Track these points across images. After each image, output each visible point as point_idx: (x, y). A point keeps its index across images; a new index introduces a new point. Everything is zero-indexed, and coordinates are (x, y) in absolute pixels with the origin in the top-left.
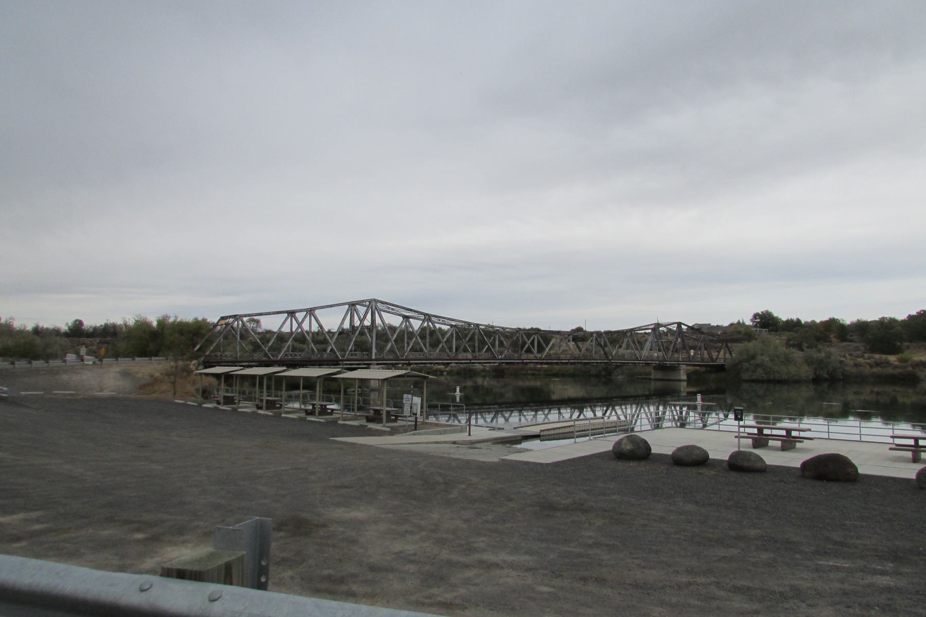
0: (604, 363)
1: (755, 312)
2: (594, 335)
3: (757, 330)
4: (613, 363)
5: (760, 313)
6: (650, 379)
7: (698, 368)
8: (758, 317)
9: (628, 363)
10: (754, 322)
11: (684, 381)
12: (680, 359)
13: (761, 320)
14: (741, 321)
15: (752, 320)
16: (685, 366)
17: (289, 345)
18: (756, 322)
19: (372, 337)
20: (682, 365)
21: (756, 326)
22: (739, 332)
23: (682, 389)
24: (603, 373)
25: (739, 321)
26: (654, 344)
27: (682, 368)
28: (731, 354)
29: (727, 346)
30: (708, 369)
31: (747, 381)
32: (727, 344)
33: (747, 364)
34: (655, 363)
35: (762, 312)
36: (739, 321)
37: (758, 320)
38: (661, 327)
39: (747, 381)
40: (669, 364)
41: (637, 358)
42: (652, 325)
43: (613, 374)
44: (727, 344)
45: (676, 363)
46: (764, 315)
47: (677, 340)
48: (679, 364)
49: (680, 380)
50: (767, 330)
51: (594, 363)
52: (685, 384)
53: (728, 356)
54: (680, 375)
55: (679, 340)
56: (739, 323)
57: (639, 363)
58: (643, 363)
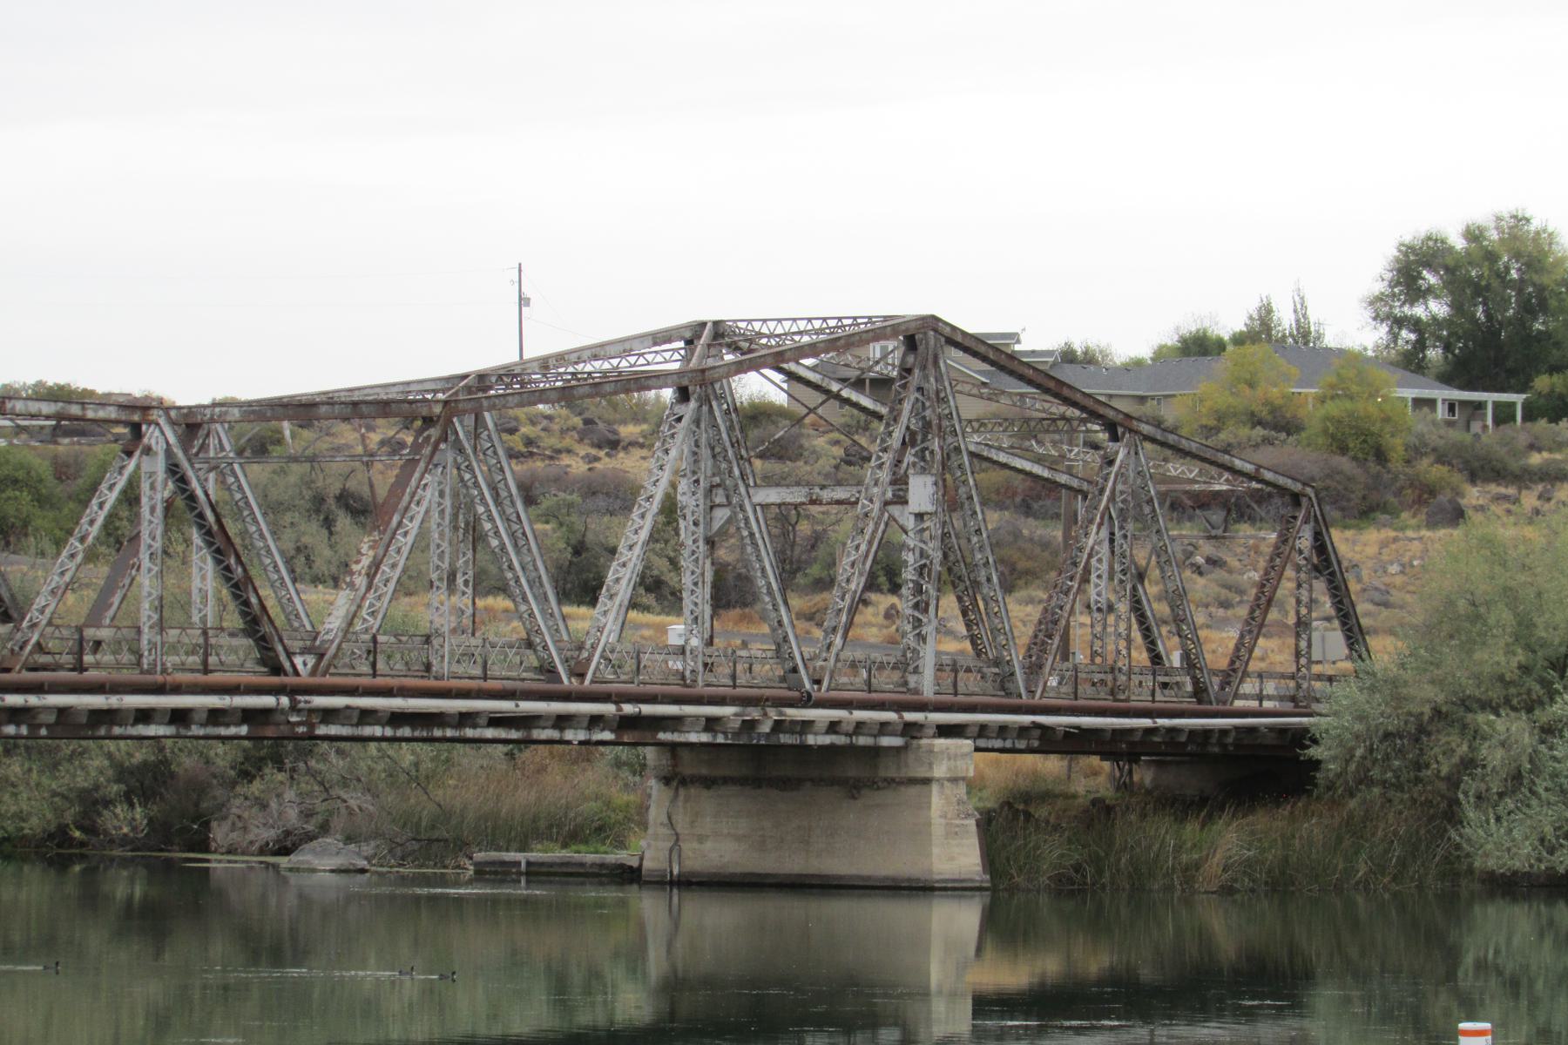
0: (248, 715)
1: (1413, 227)
2: (152, 436)
3: (1431, 403)
4: (329, 715)
5: (1459, 243)
6: (629, 876)
7: (1052, 765)
8: (1430, 278)
9: (466, 719)
10: (1399, 322)
11: (956, 889)
12: (926, 682)
13: (1457, 306)
14: (1285, 319)
15: (1381, 309)
16: (967, 744)
17: (416, 867)
18: (1416, 325)
19: (583, 618)
20: (941, 743)
21: (1412, 362)
22: (1281, 423)
23: (937, 973)
24: (124, 820)
25: (1266, 311)
26: (434, 506)
27: (940, 771)
28: (1354, 634)
29: (1325, 563)
30: (1144, 775)
31: (1507, 886)
32: (1321, 546)
33: (1515, 729)
34: (711, 724)
35: (1474, 235)
36: (1266, 311)
37: (1437, 308)
38: (755, 365)
39: (1507, 886)
40: (833, 727)
41: (549, 671)
42: (660, 338)
43: (220, 833)
44: (1321, 546)
45: (890, 716)
46: (1491, 256)
47: (902, 500)
48: (911, 730)
49: (921, 889)
50: (1518, 399)
51: (144, 716)
52: (965, 918)
53: (1330, 643)
54: (921, 834)
55: (922, 492)
56: (1261, 331)
57: (562, 721)
58: (595, 721)
